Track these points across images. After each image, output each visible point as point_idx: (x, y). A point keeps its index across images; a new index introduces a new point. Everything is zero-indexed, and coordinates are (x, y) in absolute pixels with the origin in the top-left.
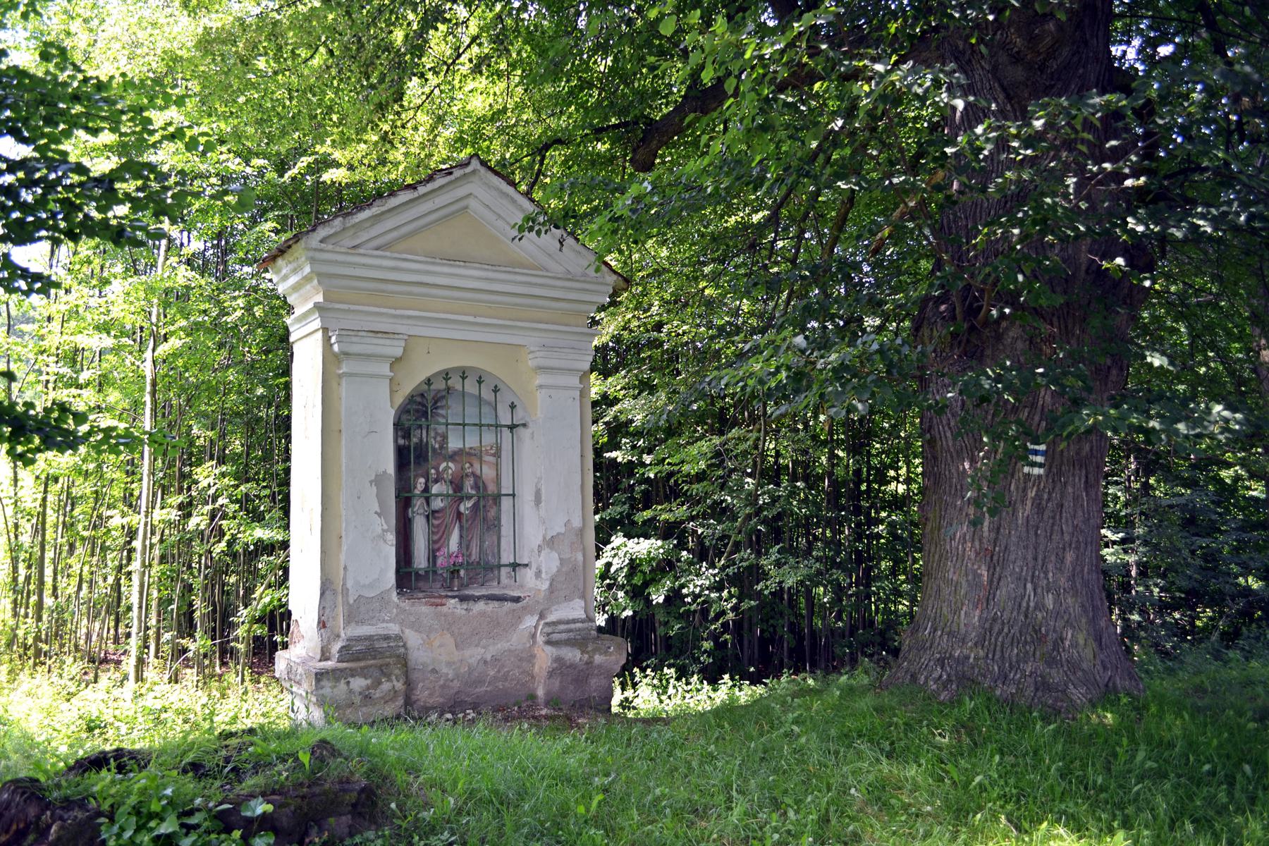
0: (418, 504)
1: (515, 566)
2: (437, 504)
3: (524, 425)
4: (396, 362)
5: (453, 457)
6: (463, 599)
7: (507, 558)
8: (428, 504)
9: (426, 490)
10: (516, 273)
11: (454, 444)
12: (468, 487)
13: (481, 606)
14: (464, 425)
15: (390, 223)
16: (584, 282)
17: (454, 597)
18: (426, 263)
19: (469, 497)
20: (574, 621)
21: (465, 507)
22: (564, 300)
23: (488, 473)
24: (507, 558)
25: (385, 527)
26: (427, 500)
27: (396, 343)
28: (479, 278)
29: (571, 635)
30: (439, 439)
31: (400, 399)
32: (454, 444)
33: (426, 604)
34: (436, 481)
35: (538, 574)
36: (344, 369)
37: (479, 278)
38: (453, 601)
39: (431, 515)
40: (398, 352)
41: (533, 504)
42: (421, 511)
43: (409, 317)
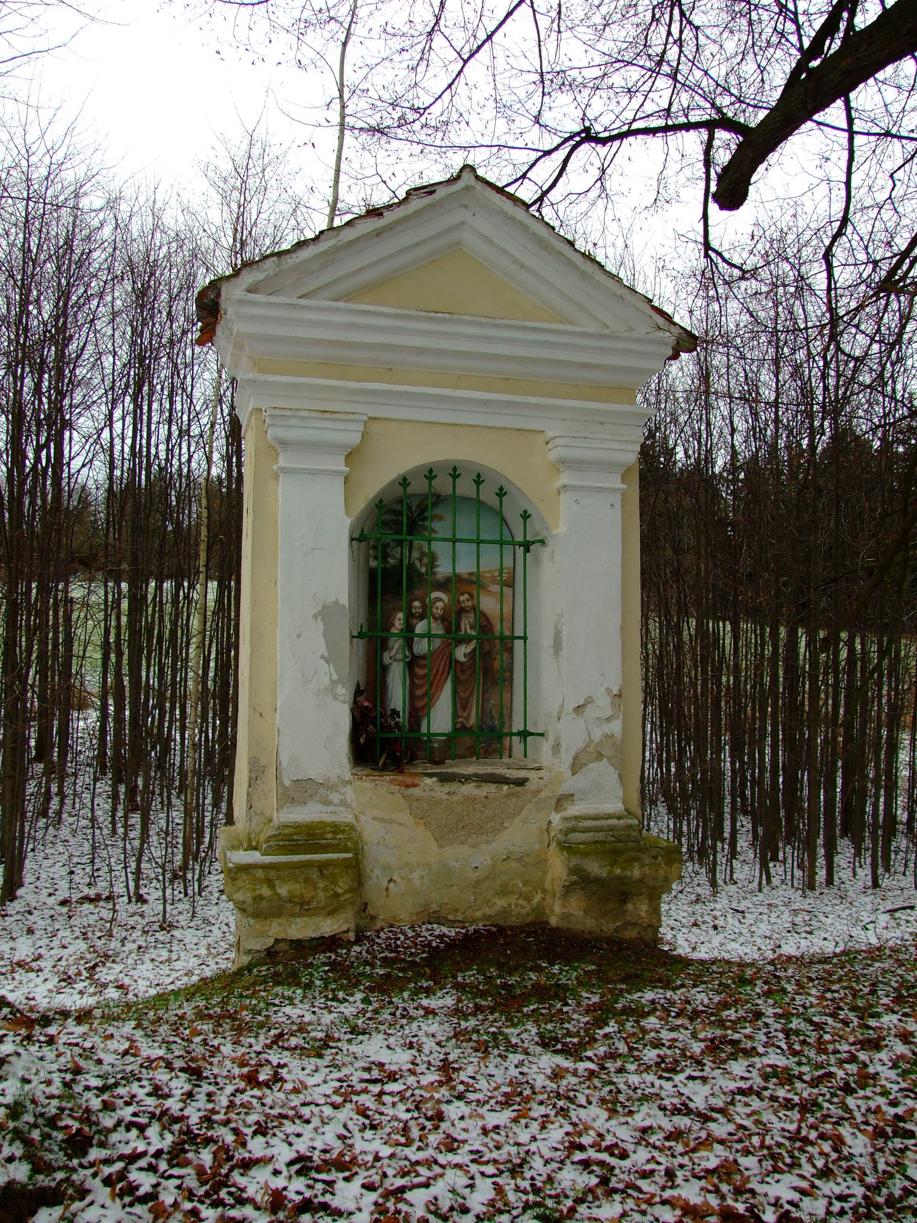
0: (396, 645)
1: (525, 734)
2: (422, 647)
3: (543, 542)
4: (352, 456)
5: (443, 585)
6: (445, 779)
7: (517, 726)
8: (411, 648)
9: (409, 628)
10: (525, 328)
11: (444, 569)
12: (467, 625)
13: (469, 789)
14: (479, 542)
15: (348, 265)
16: (629, 340)
17: (431, 775)
18: (396, 316)
19: (467, 640)
20: (609, 817)
21: (461, 653)
22: (360, 270)
23: (488, 604)
24: (517, 726)
25: (335, 677)
26: (409, 643)
27: (351, 426)
28: (472, 337)
29: (600, 836)
30: (425, 560)
31: (361, 503)
32: (444, 569)
33: (391, 782)
34: (422, 617)
35: (556, 747)
36: (283, 461)
37: (472, 337)
38: (428, 781)
39: (412, 663)
40: (355, 438)
41: (551, 651)
42: (400, 656)
43: (374, 393)
